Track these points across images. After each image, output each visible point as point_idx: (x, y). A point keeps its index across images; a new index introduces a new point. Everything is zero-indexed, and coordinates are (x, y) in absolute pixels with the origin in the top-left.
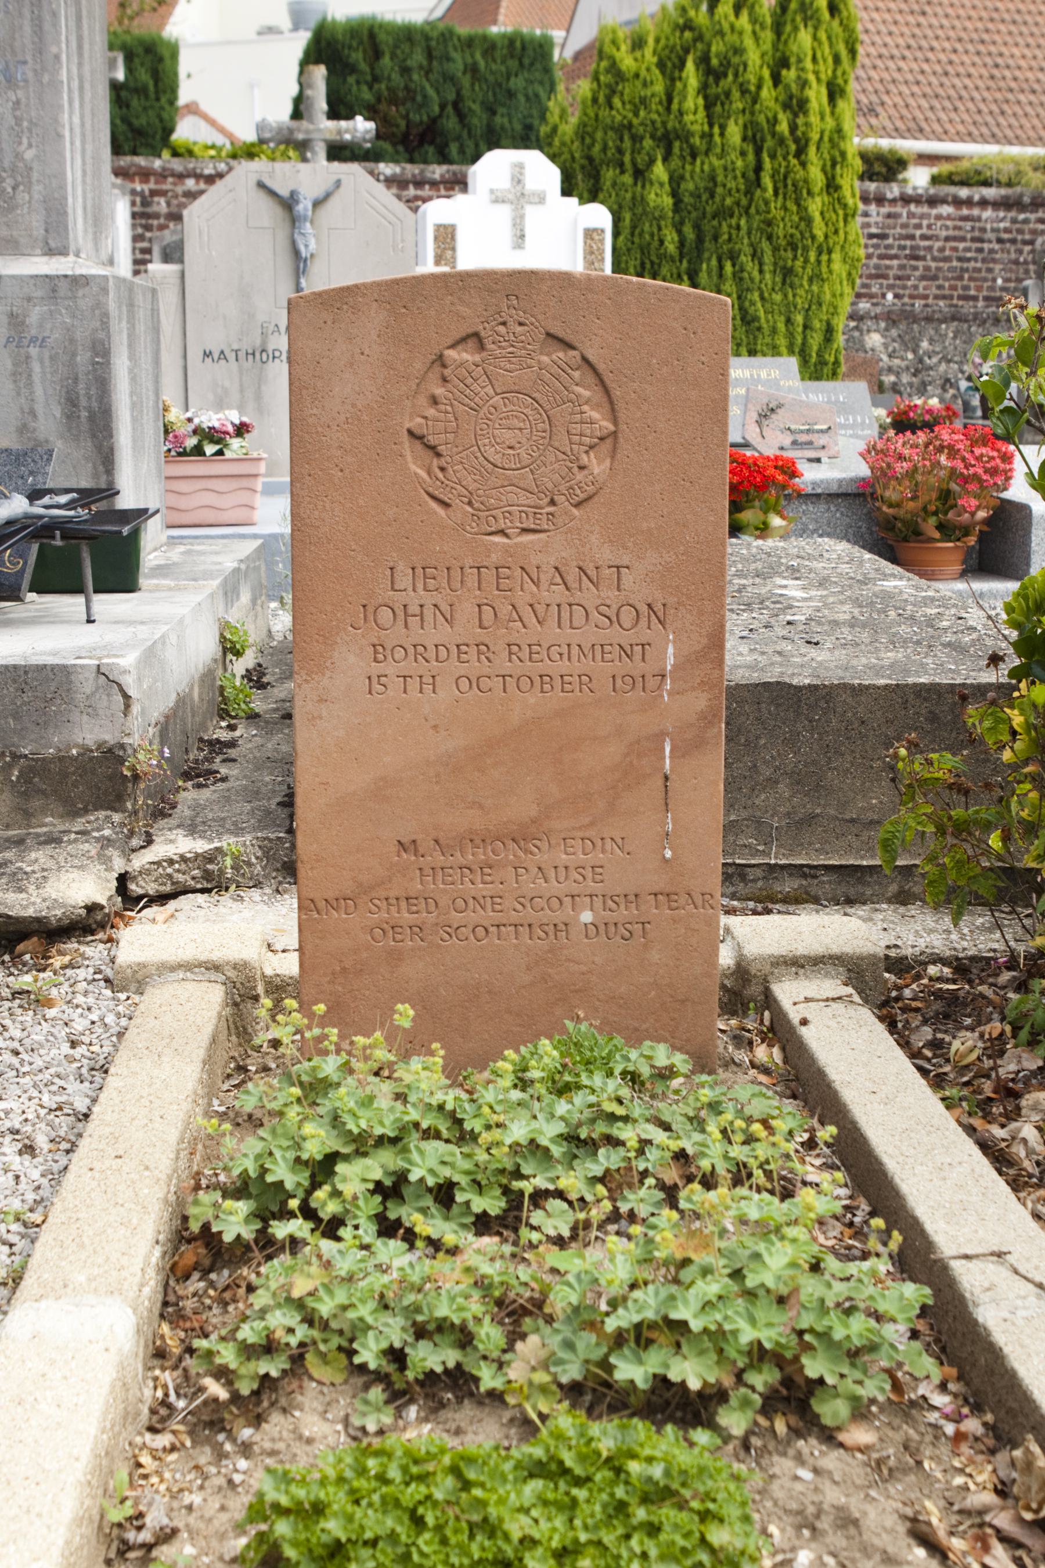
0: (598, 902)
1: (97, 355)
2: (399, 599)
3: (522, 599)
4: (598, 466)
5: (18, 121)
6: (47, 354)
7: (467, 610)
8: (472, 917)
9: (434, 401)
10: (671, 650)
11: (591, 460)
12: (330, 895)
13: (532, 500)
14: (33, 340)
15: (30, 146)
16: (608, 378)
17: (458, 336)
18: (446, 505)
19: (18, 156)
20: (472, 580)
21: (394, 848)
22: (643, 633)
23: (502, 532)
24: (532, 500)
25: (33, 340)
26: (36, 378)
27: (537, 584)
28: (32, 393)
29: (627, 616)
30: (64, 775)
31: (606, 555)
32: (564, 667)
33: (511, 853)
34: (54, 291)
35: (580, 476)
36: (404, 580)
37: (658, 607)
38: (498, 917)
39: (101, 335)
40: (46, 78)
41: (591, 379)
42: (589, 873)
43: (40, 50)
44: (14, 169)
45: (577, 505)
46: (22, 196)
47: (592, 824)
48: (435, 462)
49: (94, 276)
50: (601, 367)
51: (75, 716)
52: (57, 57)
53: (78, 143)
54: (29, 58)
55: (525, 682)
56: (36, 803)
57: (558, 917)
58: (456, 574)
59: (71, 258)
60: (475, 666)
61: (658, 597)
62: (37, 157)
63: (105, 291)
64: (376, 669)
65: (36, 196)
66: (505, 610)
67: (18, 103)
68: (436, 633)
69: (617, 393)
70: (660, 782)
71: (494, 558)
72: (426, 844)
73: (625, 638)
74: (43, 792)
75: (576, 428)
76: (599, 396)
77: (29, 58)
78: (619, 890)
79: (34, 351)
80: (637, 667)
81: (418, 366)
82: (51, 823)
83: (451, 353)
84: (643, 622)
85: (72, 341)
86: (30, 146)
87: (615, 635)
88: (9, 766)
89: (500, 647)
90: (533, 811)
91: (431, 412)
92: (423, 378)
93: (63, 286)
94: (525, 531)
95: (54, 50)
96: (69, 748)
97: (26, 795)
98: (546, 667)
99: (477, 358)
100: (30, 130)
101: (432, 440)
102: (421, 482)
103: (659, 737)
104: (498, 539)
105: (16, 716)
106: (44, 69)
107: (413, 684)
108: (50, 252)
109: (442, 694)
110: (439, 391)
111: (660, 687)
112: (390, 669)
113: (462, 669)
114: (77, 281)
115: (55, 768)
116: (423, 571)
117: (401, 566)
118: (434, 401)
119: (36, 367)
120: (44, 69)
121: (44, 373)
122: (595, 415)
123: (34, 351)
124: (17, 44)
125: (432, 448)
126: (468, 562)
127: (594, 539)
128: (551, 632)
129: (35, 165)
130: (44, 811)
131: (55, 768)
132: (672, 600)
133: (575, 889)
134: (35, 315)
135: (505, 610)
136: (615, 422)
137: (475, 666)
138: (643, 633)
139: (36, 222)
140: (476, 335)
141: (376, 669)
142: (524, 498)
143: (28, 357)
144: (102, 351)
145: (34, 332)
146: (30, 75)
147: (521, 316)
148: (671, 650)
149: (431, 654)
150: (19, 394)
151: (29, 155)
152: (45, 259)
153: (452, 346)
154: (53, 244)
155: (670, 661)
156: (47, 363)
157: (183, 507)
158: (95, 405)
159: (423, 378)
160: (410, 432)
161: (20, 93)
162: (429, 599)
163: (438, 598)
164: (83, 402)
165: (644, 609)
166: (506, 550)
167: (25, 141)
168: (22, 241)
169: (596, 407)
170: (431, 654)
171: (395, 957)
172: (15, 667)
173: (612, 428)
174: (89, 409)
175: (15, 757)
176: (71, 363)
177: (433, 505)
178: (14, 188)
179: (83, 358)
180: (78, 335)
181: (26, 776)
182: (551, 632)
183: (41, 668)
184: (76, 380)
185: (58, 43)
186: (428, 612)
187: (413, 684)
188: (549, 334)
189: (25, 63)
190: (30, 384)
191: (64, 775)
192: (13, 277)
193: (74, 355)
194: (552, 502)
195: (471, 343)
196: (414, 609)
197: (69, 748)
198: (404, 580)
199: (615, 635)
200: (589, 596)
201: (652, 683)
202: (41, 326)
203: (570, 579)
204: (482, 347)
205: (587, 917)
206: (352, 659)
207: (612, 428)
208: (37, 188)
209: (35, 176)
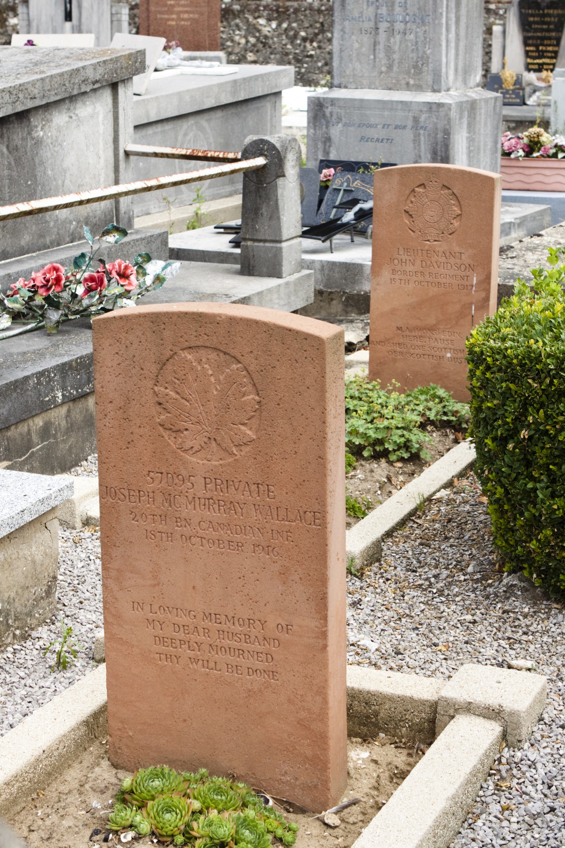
0: (452, 351)
1: (445, 135)
2: (400, 257)
3: (433, 260)
4: (456, 224)
5: (425, 38)
6: (426, 133)
7: (418, 262)
8: (417, 351)
9: (412, 202)
10: (475, 279)
11: (454, 221)
12: (378, 340)
13: (438, 232)
14: (422, 127)
15: (429, 49)
16: (460, 198)
17: (419, 184)
18: (414, 232)
19: (424, 52)
20: (420, 254)
21: (395, 328)
22: (467, 273)
23: (428, 240)
24: (438, 232)
25: (422, 127)
26: (422, 142)
27: (438, 256)
28: (420, 148)
29: (463, 267)
30: (359, 300)
31: (457, 249)
32: (444, 280)
33: (429, 334)
34: (431, 108)
35: (451, 226)
36: (401, 252)
37: (472, 266)
38: (423, 352)
39: (447, 127)
40: (437, 22)
41: (455, 198)
42: (450, 342)
43: (435, 11)
44: (422, 57)
45: (450, 234)
46: (425, 68)
47: (451, 328)
48: (411, 219)
49: (446, 104)
50: (458, 195)
51: (363, 281)
52: (441, 14)
53: (453, 45)
54: (431, 14)
55: (433, 284)
56: (349, 309)
57: (441, 354)
58: (416, 252)
59: (443, 93)
60: (420, 278)
61: (472, 263)
62: (431, 53)
63: (450, 109)
64: (393, 277)
65: (430, 69)
66: (429, 263)
67: (425, 31)
68: (409, 268)
69: (462, 203)
70: (471, 317)
71: (426, 248)
72: (404, 329)
73: (463, 274)
74: (352, 306)
75: (450, 212)
76: (457, 204)
77: (431, 14)
78: (458, 348)
79: (422, 132)
80: (465, 282)
81: (408, 192)
82: (353, 316)
83: (417, 189)
84: (467, 270)
85: (436, 129)
86: (429, 49)
87: (459, 273)
88: (342, 296)
89: (427, 274)
90: (434, 322)
91: (411, 205)
92: (409, 196)
93: (434, 107)
94: (435, 241)
95: (440, 11)
96: (361, 291)
97: (346, 306)
98: (440, 280)
99: (424, 191)
100: (429, 42)
101: (411, 213)
102: (407, 225)
103: (471, 304)
104: (427, 242)
105: (346, 279)
106: (436, 18)
107: (403, 282)
108: (434, 91)
109: (410, 285)
110: (413, 199)
111: (472, 289)
112: (397, 277)
113: (416, 279)
114: (440, 105)
115: (356, 297)
116: (406, 250)
117: (401, 248)
118: (412, 202)
119: (422, 138)
120: (436, 18)
121: (425, 141)
122: (456, 209)
123: (422, 132)
124: (427, 8)
125: (411, 215)
126: (419, 248)
127: (454, 244)
128: (442, 270)
129: (431, 56)
130: (352, 312)
131: (356, 297)
132: (475, 264)
133: (446, 346)
134: (423, 117)
135: (429, 263)
136: (461, 211)
137: (420, 278)
138: (467, 273)
139: (429, 79)
140: (423, 184)
141: (393, 277)
142: (435, 231)
143: (419, 134)
144: (447, 133)
145: (422, 124)
146: (431, 20)
147: (436, 179)
148: (475, 279)
149: (408, 274)
150: (415, 148)
151: (429, 52)
152: (432, 94)
153: (417, 187)
154: (435, 88)
155: (475, 282)
156: (426, 137)
157: (546, 182)
158: (443, 154)
159: (409, 196)
160: (405, 211)
161: (427, 28)
162: (408, 258)
163: (410, 258)
164: (439, 153)
165: (468, 266)
166: (430, 246)
167: (427, 46)
168: (424, 86)
169: (457, 206)
170: (408, 274)
171: (395, 361)
172: (346, 263)
173: (459, 212)
174: (441, 156)
175: (344, 293)
176: (435, 138)
177: (410, 231)
178: (422, 65)
179: (440, 135)
180: (439, 126)
181: (347, 299)
182: (442, 270)
183: (354, 264)
184: (437, 144)
185: (442, 8)
186: (408, 262)
187: (403, 282)
188: (444, 185)
189: (429, 15)
190: (419, 145)
191: (359, 300)
192: (416, 102)
193: (437, 134)
194: (443, 233)
195: (422, 186)
196: (404, 260)
197: (361, 291)
198: (401, 252)
199: (459, 273)
200: (452, 261)
201: (469, 288)
202: (425, 122)
203: (447, 255)
204: (425, 188)
205: (449, 355)
206: (386, 273)
207: (459, 212)
208: (431, 65)
209: (430, 60)
